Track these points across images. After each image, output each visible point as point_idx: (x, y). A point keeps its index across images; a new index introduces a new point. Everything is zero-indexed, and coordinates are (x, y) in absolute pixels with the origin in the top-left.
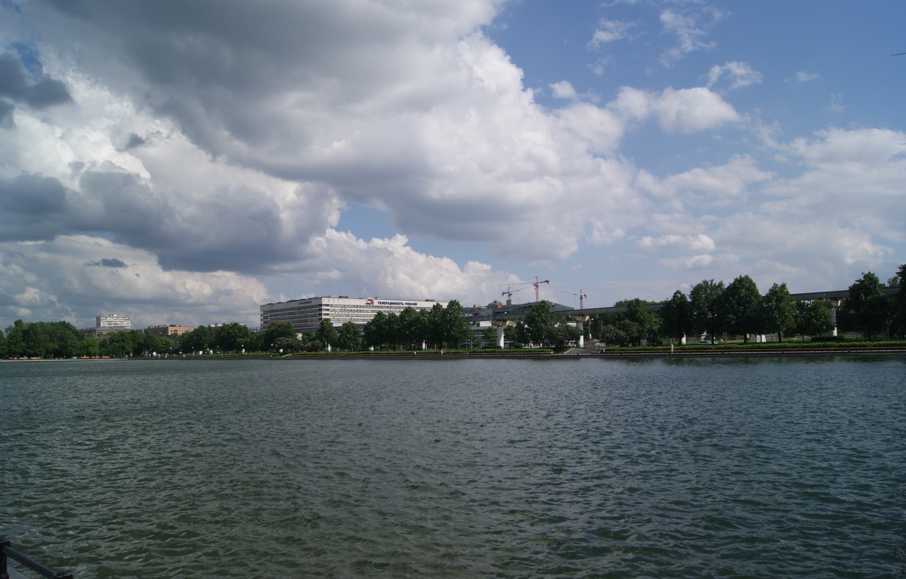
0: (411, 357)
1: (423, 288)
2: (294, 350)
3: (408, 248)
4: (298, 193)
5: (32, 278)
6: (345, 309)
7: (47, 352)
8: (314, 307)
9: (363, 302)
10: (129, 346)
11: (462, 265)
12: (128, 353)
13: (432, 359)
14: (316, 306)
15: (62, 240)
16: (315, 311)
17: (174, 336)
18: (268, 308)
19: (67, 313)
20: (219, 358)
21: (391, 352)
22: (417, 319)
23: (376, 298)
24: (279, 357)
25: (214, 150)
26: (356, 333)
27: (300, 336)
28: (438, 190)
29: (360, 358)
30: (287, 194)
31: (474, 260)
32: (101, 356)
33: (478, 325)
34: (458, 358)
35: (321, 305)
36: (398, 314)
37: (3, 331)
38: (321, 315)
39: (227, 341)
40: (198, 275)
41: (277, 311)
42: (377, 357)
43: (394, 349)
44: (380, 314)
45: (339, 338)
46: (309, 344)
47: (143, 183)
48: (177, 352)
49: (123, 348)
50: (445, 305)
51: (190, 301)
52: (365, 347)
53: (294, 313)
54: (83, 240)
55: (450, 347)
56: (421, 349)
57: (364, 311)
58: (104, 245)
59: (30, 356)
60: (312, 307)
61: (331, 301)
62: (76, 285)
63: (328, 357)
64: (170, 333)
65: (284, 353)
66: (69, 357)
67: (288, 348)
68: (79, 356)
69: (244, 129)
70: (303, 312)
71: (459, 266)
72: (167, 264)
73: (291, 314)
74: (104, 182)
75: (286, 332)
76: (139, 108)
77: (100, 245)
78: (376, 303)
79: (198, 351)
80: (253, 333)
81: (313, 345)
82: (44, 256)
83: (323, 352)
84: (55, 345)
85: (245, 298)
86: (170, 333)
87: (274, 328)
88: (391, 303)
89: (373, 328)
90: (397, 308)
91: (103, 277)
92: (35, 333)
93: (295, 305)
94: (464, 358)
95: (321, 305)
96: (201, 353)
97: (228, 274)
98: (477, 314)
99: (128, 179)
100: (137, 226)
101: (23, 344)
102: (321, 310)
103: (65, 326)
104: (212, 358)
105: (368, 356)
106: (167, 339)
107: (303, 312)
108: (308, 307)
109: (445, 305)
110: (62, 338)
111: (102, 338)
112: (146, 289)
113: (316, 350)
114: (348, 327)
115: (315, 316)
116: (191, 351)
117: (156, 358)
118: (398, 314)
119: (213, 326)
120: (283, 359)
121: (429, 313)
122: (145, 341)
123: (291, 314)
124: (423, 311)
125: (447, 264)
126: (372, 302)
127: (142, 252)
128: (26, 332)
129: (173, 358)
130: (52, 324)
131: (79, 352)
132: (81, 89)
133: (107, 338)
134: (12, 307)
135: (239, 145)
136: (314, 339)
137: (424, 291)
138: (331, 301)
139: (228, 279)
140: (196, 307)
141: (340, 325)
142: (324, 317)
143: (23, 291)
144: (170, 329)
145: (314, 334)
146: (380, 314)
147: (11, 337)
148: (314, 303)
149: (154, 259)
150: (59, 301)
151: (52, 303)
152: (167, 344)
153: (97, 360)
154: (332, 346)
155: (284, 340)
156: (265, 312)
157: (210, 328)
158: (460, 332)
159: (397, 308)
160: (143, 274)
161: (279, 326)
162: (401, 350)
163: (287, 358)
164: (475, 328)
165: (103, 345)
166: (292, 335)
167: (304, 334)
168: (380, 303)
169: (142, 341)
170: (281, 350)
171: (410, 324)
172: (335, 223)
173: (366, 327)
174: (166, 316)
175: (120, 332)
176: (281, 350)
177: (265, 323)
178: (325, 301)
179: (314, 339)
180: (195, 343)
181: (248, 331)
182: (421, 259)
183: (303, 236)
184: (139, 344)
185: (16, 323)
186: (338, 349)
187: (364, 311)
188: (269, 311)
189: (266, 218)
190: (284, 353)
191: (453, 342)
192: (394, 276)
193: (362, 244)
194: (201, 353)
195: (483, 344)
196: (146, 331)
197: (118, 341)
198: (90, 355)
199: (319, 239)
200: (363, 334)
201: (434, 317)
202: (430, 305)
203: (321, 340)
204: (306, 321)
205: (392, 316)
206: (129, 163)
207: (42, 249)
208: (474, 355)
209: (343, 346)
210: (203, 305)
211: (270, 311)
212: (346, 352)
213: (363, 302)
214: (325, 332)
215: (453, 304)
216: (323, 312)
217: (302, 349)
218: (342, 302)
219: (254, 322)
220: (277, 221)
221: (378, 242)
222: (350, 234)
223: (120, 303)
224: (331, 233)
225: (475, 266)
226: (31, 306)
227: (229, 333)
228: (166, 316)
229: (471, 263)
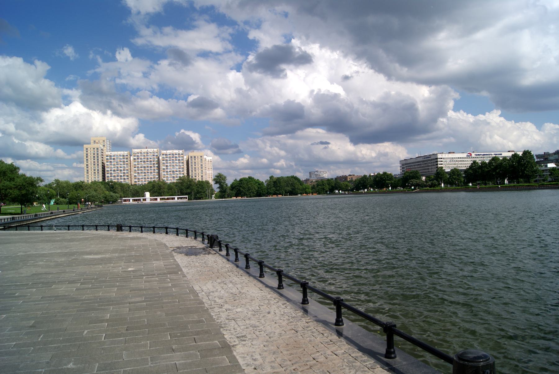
0: (498, 190)
1: (510, 144)
2: (421, 187)
3: (502, 119)
4: (431, 92)
5: (283, 153)
6: (453, 160)
7: (286, 192)
8: (433, 160)
9: (465, 155)
10: (327, 187)
11: (539, 126)
12: (327, 191)
13: (525, 190)
14: (434, 159)
15: (299, 133)
16: (434, 162)
17: (351, 181)
18: (404, 162)
19: (299, 172)
20: (376, 193)
21: (483, 186)
22: (501, 164)
23: (473, 152)
24: (412, 192)
25: (389, 76)
26: (459, 175)
27: (424, 178)
28: (528, 80)
29: (464, 191)
30: (424, 92)
31: (547, 122)
32: (312, 193)
33: (546, 166)
34: (530, 189)
35: (437, 159)
36: (487, 162)
37: (264, 182)
38: (437, 164)
39: (381, 182)
40: (369, 146)
41: (410, 163)
42: (473, 190)
43: (486, 184)
44: (475, 162)
45: (449, 179)
46: (430, 183)
47: (342, 97)
48: (352, 190)
49: (324, 189)
50: (520, 154)
51: (364, 161)
52: (466, 184)
53: (421, 165)
54: (311, 131)
55: (526, 182)
56: (504, 184)
57: (465, 161)
58: (319, 133)
59: (277, 194)
60: (432, 160)
61: (444, 156)
62: (306, 157)
63: (442, 190)
64: (348, 180)
65: (415, 189)
66: (297, 194)
67: (416, 185)
68: (301, 194)
69: (407, 61)
70: (426, 164)
71: (537, 128)
72: (357, 140)
73: (419, 165)
74: (321, 99)
75: (415, 175)
76: (332, 52)
77: (319, 132)
78: (473, 155)
79: (364, 189)
80: (395, 178)
81: (432, 184)
82: (290, 142)
83: (439, 188)
84: (289, 189)
85: (390, 157)
86: (348, 180)
87: (407, 174)
88: (484, 155)
89: (470, 171)
90: (488, 157)
91: (319, 151)
92: (280, 183)
93: (421, 159)
94: (535, 189)
95: (437, 159)
96: (366, 190)
97: (386, 144)
98: (546, 158)
99: (336, 96)
100: (339, 122)
101: (274, 188)
102: (437, 162)
103: (296, 178)
104: (372, 193)
105: (468, 190)
106: (346, 183)
107: (426, 164)
108: (429, 160)
109: (520, 154)
110: (292, 185)
111: (313, 184)
112: (345, 155)
113: (434, 187)
114: (455, 172)
115: (434, 165)
116: (360, 189)
117: (342, 194)
118: (487, 162)
119: (372, 174)
120: (414, 192)
121: (509, 160)
122: (335, 184)
123: (419, 165)
124: (505, 158)
125: (529, 126)
126: (471, 155)
127: (340, 135)
128: (275, 182)
129: (351, 194)
130: (287, 177)
131: (301, 191)
132: (314, 49)
133: (315, 184)
134: (273, 169)
135: (405, 71)
136: (433, 180)
137: (511, 146)
138: (444, 156)
139: (387, 147)
140: (368, 163)
141: (449, 170)
142: (439, 166)
143: (278, 161)
144: (349, 177)
145: (433, 177)
146: (475, 162)
147: (268, 185)
148: (433, 157)
149: (348, 139)
150: (296, 165)
151: (292, 166)
152: (347, 186)
153: (310, 196)
154: (444, 184)
155: (414, 181)
156: (403, 165)
157: (370, 176)
158: (532, 172)
159: (488, 157)
160: (341, 147)
161: (411, 173)
162: (491, 184)
163: (416, 192)
164: (544, 168)
165: (313, 188)
166: (419, 178)
167: (426, 177)
168: (476, 155)
169: (333, 185)
170: (413, 187)
171: (496, 167)
172: (452, 108)
173: (466, 171)
174: (350, 170)
175: (322, 180)
176: (413, 187)
177: (403, 171)
178: (439, 156)
179: (433, 180)
180: (360, 185)
181: (392, 176)
182: (509, 124)
183: (434, 119)
184: (332, 186)
185: (270, 178)
186: (449, 186)
187: (465, 161)
188: (405, 164)
189: (411, 108)
190: (415, 189)
191: (528, 178)
192: (491, 137)
193: (471, 118)
194: (366, 190)
195: (549, 179)
196: (336, 179)
197: (320, 185)
198: (307, 193)
199: (441, 120)
200: (464, 175)
201: (513, 162)
202: (510, 154)
203: (437, 180)
204: (428, 169)
205: (483, 163)
206: (337, 89)
207: (291, 138)
208: (542, 187)
209: (452, 184)
210: (370, 162)
211: (406, 164)
212: (454, 187)
213: (465, 155)
214: (440, 175)
215: (527, 153)
216: (439, 163)
217: (426, 186)
218: (451, 156)
219: (396, 170)
220: (417, 110)
221: (481, 117)
222: (462, 112)
223: (327, 163)
224: (451, 113)
225: (549, 127)
226: (281, 168)
227: (381, 178)
228: (350, 170)
229: (546, 124)
